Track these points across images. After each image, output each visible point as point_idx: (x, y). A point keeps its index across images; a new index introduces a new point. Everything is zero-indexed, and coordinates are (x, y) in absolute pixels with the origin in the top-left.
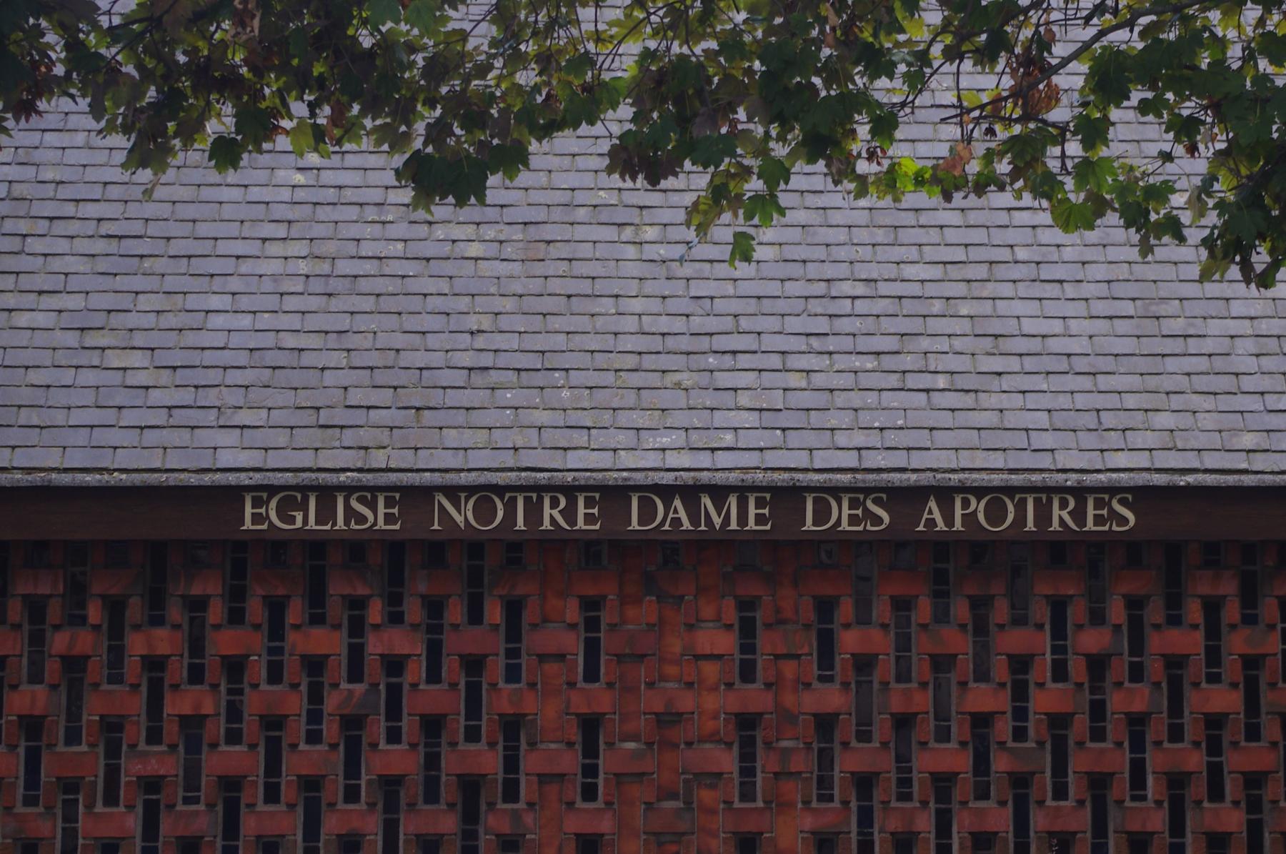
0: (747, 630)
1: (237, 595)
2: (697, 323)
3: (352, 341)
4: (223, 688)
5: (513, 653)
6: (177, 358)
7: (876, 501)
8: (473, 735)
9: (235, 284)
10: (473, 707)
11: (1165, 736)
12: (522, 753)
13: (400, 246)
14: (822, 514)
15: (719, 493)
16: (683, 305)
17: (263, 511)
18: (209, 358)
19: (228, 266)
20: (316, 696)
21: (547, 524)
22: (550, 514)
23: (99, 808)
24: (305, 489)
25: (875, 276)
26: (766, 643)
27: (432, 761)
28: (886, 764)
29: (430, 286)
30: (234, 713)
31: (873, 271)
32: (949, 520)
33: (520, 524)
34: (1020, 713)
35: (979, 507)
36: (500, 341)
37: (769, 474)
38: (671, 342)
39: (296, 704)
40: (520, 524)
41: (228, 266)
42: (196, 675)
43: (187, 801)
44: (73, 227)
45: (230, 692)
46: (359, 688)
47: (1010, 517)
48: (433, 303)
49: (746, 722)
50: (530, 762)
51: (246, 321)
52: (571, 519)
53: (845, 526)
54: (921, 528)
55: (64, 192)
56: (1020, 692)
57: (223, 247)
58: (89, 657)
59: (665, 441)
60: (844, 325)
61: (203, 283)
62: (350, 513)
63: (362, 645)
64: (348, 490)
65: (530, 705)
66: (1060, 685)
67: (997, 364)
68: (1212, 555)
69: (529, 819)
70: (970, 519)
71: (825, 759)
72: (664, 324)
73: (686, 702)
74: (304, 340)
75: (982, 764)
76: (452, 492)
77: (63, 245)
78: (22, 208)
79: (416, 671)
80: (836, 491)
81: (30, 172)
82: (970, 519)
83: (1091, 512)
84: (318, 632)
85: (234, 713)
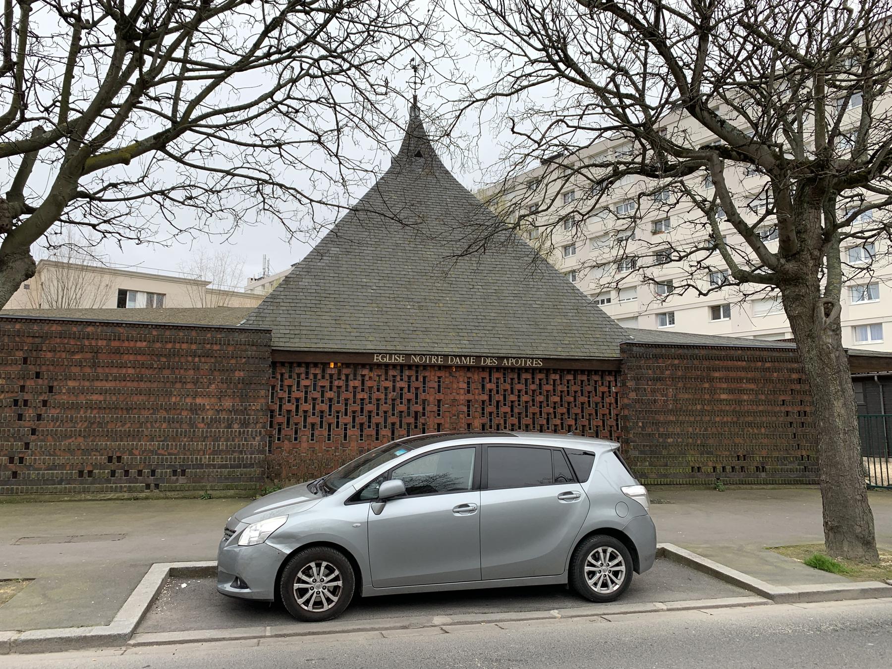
0: (468, 383)
1: (307, 373)
2: (454, 323)
3: (388, 324)
10: (417, 398)
15: (466, 357)
27: (409, 408)
29: (402, 314)
30: (370, 398)
35: (514, 361)
36: (417, 325)
42: (363, 390)
46: (395, 393)
49: (469, 401)
50: (428, 409)
51: (367, 319)
52: (437, 361)
55: (326, 292)
60: (481, 324)
61: (357, 312)
62: (395, 358)
64: (395, 354)
65: (428, 397)
67: (511, 333)
68: (555, 371)
69: (428, 420)
70: (512, 363)
71: (483, 409)
72: (447, 323)
73: (457, 397)
74: (379, 324)
75: (512, 411)
76: (415, 355)
77: (328, 303)
79: (406, 390)
80: (487, 357)
82: (512, 363)
85: (370, 398)
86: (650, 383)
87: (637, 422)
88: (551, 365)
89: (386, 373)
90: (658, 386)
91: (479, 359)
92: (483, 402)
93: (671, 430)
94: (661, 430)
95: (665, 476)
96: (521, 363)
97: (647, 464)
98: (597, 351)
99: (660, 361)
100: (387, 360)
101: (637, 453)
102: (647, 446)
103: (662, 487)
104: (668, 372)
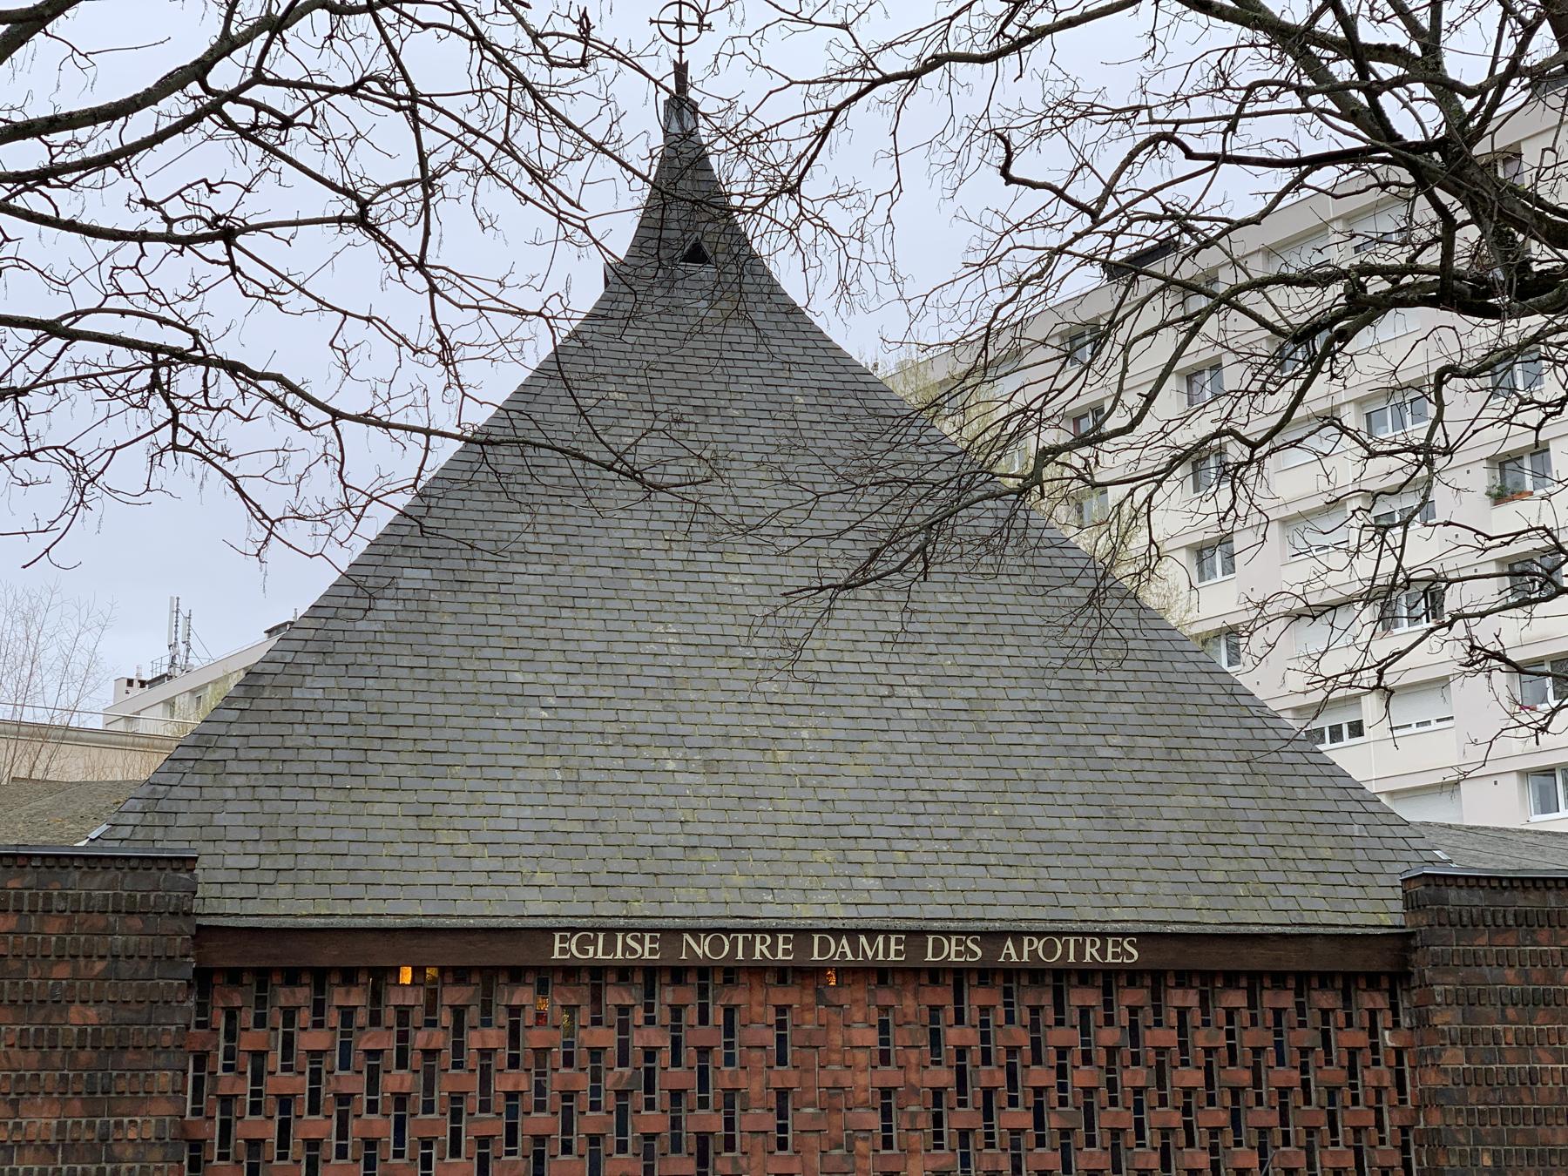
0: (884, 1027)
3: (601, 826)
4: (533, 1072)
5: (728, 1045)
6: (487, 837)
7: (1130, 943)
8: (703, 1103)
9: (515, 786)
11: (1205, 1104)
12: (737, 1116)
13: (621, 762)
14: (938, 949)
15: (871, 934)
16: (816, 806)
17: (567, 945)
18: (509, 837)
19: (508, 773)
20: (596, 1077)
21: (757, 956)
22: (760, 949)
23: (448, 1160)
24: (595, 930)
25: (934, 787)
26: (898, 1037)
27: (676, 1123)
28: (978, 1122)
29: (649, 789)
30: (540, 1090)
31: (932, 785)
32: (1020, 954)
33: (740, 956)
34: (1062, 1088)
35: (1039, 945)
36: (702, 828)
37: (897, 922)
38: (813, 830)
39: (584, 1083)
40: (740, 956)
41: (508, 773)
43: (508, 1153)
44: (399, 745)
45: (537, 1074)
46: (627, 1071)
47: (1059, 952)
48: (650, 801)
49: (886, 1093)
52: (1104, 956)
53: (953, 958)
54: (1002, 960)
56: (1062, 1072)
57: (503, 760)
58: (440, 1050)
59: (824, 899)
60: (923, 820)
62: (625, 946)
63: (627, 1040)
64: (626, 930)
65: (742, 1082)
66: (1087, 1068)
68: (1183, 979)
69: (744, 1163)
71: (938, 1120)
73: (846, 1079)
75: (1039, 1123)
76: (694, 932)
77: (393, 757)
78: (361, 731)
80: (947, 933)
81: (362, 706)
82: (1033, 953)
83: (1110, 950)
84: (598, 1030)
85: (540, 1090)
86: (1511, 1012)
88: (1166, 958)
90: (1541, 1022)
91: (918, 940)
92: (938, 1093)
96: (1066, 953)
99: (1543, 935)
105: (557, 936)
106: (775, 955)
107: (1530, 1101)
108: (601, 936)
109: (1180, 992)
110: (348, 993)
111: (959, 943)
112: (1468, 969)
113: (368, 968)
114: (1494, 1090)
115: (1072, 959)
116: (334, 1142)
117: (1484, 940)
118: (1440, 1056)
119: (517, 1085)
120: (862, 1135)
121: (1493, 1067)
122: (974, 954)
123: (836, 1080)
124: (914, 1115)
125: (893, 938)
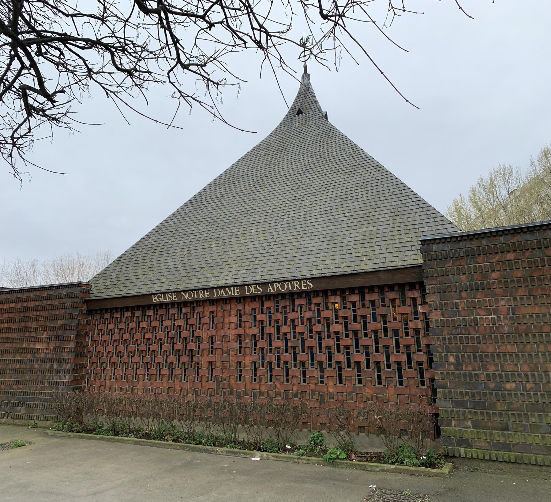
0: (241, 316)
14: (249, 290)
15: (229, 287)
35: (279, 286)
49: (240, 336)
52: (301, 287)
53: (253, 292)
70: (278, 288)
71: (255, 344)
76: (184, 291)
80: (251, 285)
82: (278, 288)
86: (464, 294)
87: (447, 357)
88: (323, 286)
89: (363, 298)
90: (479, 297)
91: (242, 288)
92: (254, 336)
93: (509, 368)
94: (492, 368)
95: (506, 447)
96: (288, 287)
97: (470, 423)
98: (397, 259)
99: (480, 259)
100: (162, 300)
101: (450, 405)
102: (467, 394)
103: (502, 466)
104: (495, 275)
105: (153, 296)
106: (205, 296)
107: (474, 333)
108: (162, 295)
109: (333, 297)
110: (335, 298)
111: (255, 288)
112: (442, 277)
113: (368, 287)
114: (456, 329)
115: (290, 289)
116: (374, 346)
117: (450, 264)
118: (429, 315)
119: (149, 337)
120: (233, 349)
121: (455, 318)
122: (260, 291)
123: (225, 333)
124: (247, 343)
125: (235, 288)
